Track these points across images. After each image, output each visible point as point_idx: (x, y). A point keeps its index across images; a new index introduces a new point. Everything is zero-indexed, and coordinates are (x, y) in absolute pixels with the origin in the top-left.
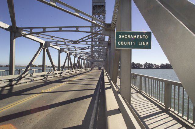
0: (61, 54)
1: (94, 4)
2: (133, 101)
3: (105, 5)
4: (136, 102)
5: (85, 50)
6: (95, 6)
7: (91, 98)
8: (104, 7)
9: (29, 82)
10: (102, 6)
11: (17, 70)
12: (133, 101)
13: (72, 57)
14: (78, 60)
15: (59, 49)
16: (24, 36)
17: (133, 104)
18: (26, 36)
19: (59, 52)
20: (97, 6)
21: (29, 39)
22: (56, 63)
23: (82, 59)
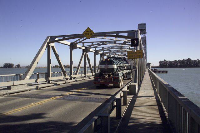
0: (74, 51)
2: (133, 115)
3: (146, 29)
4: (154, 115)
5: (101, 42)
8: (146, 30)
11: (36, 74)
12: (133, 115)
13: (91, 55)
14: (101, 57)
15: (69, 44)
16: (79, 48)
17: (158, 115)
18: (81, 48)
19: (94, 54)
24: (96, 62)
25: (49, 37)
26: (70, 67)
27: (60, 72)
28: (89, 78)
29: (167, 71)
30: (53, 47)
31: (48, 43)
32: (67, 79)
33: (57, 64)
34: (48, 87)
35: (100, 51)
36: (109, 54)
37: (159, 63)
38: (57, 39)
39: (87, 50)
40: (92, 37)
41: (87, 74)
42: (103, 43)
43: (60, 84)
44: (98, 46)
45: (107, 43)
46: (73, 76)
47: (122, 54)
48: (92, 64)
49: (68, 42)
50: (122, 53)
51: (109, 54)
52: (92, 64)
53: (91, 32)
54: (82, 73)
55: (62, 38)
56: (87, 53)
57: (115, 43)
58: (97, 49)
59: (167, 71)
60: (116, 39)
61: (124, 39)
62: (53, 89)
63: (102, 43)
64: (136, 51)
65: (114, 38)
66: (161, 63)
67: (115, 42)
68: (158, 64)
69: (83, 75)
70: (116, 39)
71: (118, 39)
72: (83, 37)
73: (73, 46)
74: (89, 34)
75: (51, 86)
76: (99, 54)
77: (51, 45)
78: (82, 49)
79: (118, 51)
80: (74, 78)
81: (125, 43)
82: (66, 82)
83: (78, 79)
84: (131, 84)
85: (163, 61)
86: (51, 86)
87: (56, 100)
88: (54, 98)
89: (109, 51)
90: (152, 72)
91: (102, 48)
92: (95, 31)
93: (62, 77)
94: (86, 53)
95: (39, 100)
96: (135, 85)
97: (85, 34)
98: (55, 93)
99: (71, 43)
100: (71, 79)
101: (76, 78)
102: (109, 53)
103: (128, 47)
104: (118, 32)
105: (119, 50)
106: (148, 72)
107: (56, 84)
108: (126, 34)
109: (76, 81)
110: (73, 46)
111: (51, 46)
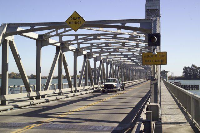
0: (44, 50)
1: (148, 8)
3: (160, 9)
5: (90, 35)
6: (148, 10)
7: (118, 124)
9: (64, 98)
10: (157, 10)
13: (69, 56)
14: (57, 53)
20: (150, 10)
21: (30, 39)
22: (29, 69)
23: (77, 52)
24: (42, 64)
25: (5, 24)
26: (37, 77)
27: (18, 86)
28: (67, 97)
29: (198, 86)
30: (11, 43)
31: (5, 36)
32: (31, 98)
33: (17, 71)
34: (3, 111)
35: (69, 43)
36: (98, 55)
37: (182, 71)
38: (19, 29)
39: (62, 47)
40: (81, 28)
41: (78, 88)
42: (95, 37)
43: (21, 107)
44: (65, 31)
45: (102, 37)
46: (42, 93)
47: (121, 54)
48: (71, 73)
49: (35, 35)
50: (122, 53)
51: (98, 55)
52: (71, 73)
53: (80, 20)
54: (53, 87)
55: (29, 28)
56: (64, 53)
57: (115, 37)
58: (64, 39)
59: (198, 86)
60: (119, 31)
61: (132, 31)
62: (16, 115)
63: (92, 37)
64: (156, 53)
65: (115, 30)
66: (186, 70)
67: (115, 36)
68: (180, 74)
69: (57, 91)
70: (119, 31)
71: (122, 31)
72: (65, 28)
73: (42, 42)
74: (76, 23)
75: (7, 110)
76: (83, 54)
77: (9, 38)
78: (55, 46)
79: (115, 50)
80: (43, 96)
81: (132, 38)
82: (32, 103)
83: (50, 99)
84: (150, 104)
85: (190, 67)
86: (7, 110)
87: (35, 130)
88: (32, 127)
89: (89, 45)
90: (176, 86)
91: (74, 38)
92: (87, 18)
93: (24, 95)
94: (63, 52)
95: (7, 130)
96: (158, 106)
97: (70, 23)
98: (24, 119)
99: (40, 36)
100: (38, 97)
101: (46, 96)
102: (100, 53)
103: (135, 44)
104: (124, 22)
105: (111, 43)
106: (165, 87)
107: (17, 107)
108: (137, 25)
109: (47, 101)
110: (42, 42)
111: (8, 41)
